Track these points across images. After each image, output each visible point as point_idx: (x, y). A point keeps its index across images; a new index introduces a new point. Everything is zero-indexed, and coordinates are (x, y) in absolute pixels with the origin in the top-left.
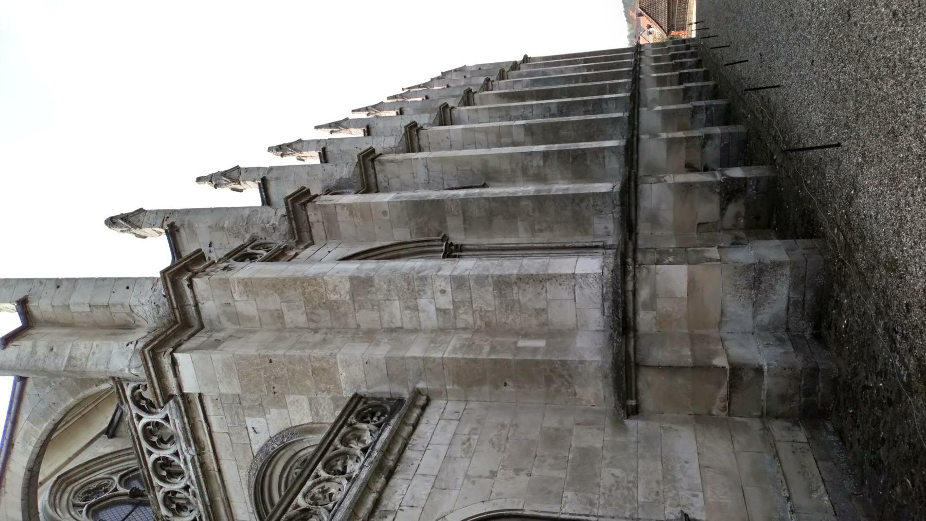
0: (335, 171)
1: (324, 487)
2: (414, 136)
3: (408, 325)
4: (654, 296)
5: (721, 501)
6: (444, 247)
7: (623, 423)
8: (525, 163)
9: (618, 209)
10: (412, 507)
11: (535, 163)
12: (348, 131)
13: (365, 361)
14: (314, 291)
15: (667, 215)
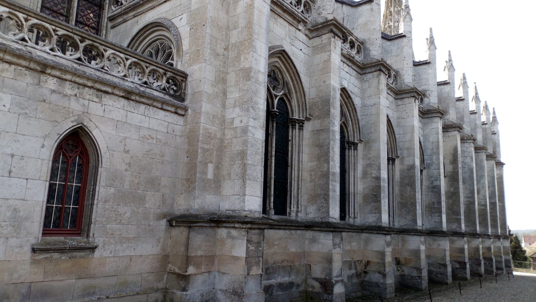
0: (376, 46)
1: (121, 63)
2: (410, 94)
3: (228, 102)
4: (233, 238)
5: (107, 265)
6: (301, 119)
7: (164, 218)
8: (374, 166)
9: (320, 220)
10: (104, 111)
11: (374, 172)
12: (427, 50)
13: (201, 79)
14: (246, 46)
15: (316, 248)
